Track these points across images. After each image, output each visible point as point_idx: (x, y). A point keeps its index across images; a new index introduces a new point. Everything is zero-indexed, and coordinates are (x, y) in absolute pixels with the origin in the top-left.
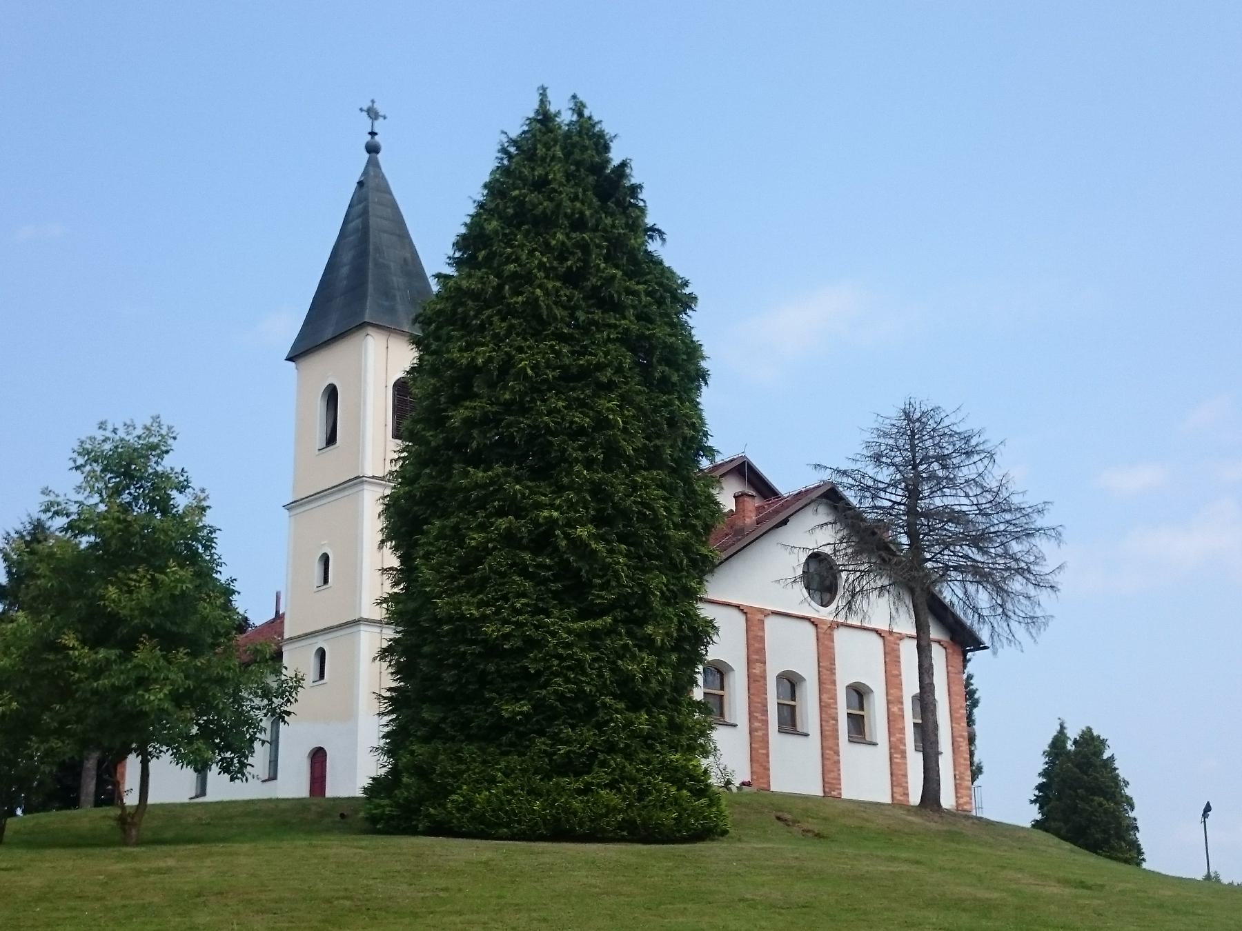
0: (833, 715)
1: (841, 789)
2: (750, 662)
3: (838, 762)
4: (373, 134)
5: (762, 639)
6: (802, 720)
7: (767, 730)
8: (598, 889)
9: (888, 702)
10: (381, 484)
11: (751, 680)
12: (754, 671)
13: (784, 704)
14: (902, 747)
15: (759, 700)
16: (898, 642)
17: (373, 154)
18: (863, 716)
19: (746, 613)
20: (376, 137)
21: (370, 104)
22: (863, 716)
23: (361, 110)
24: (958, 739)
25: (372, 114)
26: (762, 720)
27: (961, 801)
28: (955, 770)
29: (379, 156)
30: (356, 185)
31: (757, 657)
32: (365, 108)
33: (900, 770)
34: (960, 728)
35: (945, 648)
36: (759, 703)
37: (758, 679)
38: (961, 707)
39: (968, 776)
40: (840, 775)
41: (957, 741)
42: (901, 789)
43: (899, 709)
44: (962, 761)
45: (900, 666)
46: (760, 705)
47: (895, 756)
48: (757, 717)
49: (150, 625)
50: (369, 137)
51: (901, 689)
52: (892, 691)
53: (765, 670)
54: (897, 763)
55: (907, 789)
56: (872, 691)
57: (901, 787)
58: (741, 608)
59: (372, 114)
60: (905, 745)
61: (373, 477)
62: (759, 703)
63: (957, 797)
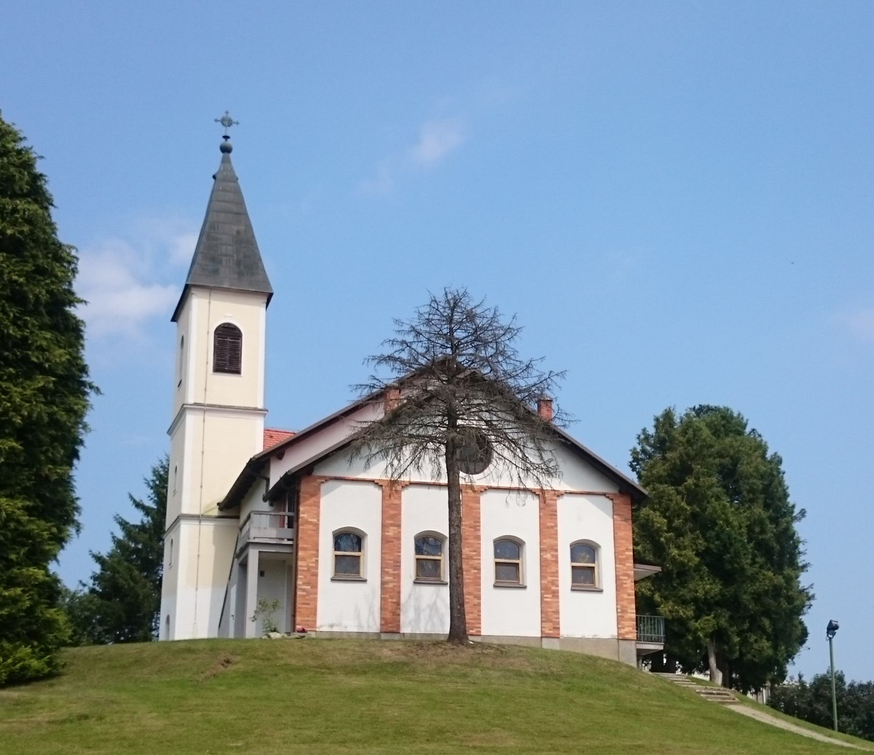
0: (475, 565)
1: (480, 628)
2: (384, 526)
3: (479, 604)
4: (226, 137)
5: (398, 507)
6: (364, 572)
7: (399, 582)
8: (471, 745)
9: (541, 550)
10: (201, 409)
11: (384, 542)
12: (387, 533)
13: (429, 560)
14: (554, 588)
15: (392, 558)
16: (555, 498)
17: (226, 154)
18: (593, 568)
19: (381, 486)
20: (229, 140)
21: (225, 115)
22: (593, 568)
23: (216, 120)
24: (622, 577)
25: (227, 122)
26: (394, 574)
27: (622, 631)
28: (617, 604)
29: (231, 155)
30: (238, 175)
31: (391, 522)
32: (220, 119)
33: (551, 608)
34: (625, 568)
35: (612, 499)
36: (390, 560)
37: (391, 540)
38: (627, 550)
39: (632, 609)
40: (480, 615)
41: (620, 579)
42: (551, 624)
43: (553, 556)
44: (626, 596)
45: (556, 519)
46: (392, 562)
47: (546, 596)
48: (388, 572)
49: (589, 558)
50: (224, 140)
51: (556, 539)
52: (544, 541)
53: (400, 532)
54: (547, 602)
55: (558, 623)
56: (600, 547)
57: (551, 621)
58: (376, 482)
59: (227, 122)
60: (557, 586)
61: (196, 404)
62: (390, 560)
63: (618, 628)
